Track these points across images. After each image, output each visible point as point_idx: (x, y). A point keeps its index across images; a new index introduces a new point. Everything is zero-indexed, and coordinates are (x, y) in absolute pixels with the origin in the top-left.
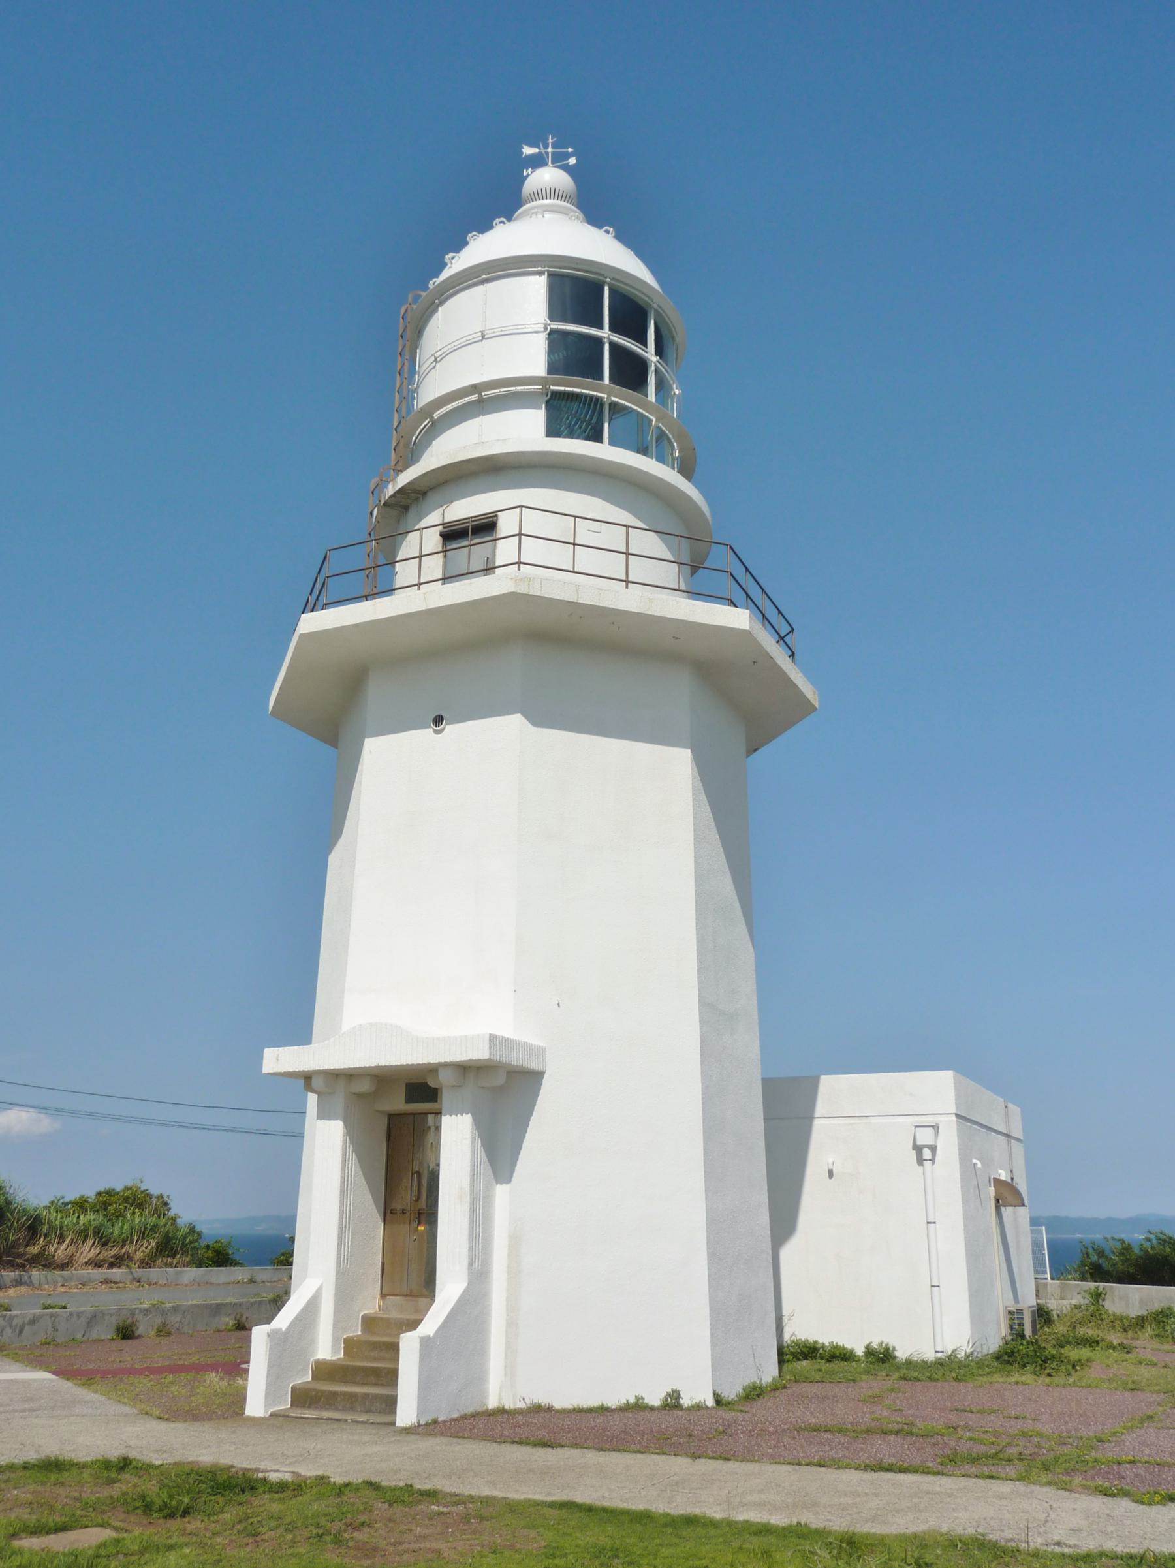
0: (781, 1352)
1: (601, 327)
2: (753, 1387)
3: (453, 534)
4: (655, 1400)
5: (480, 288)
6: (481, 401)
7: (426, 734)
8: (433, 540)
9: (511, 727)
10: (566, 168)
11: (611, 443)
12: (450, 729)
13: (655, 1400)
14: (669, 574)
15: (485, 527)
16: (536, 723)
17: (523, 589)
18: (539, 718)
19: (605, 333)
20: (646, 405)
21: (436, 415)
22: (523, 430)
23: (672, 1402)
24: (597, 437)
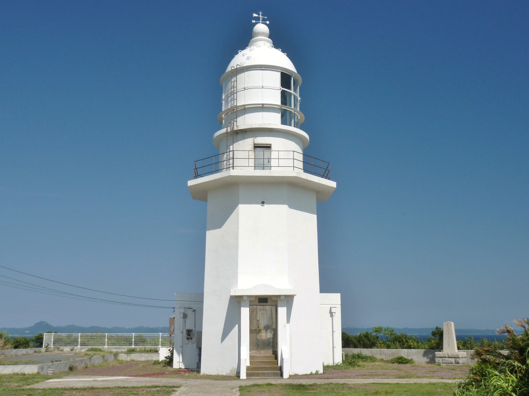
0: (324, 367)
1: (290, 88)
2: (401, 358)
3: (256, 147)
4: (314, 372)
5: (261, 71)
6: (262, 107)
7: (259, 206)
8: (251, 147)
9: (284, 208)
10: (266, 24)
11: (294, 127)
12: (266, 206)
13: (314, 372)
14: (301, 165)
15: (268, 147)
16: (290, 207)
17: (298, 176)
18: (291, 207)
19: (292, 91)
20: (292, 109)
21: (246, 107)
22: (273, 120)
23: (317, 373)
24: (290, 125)
